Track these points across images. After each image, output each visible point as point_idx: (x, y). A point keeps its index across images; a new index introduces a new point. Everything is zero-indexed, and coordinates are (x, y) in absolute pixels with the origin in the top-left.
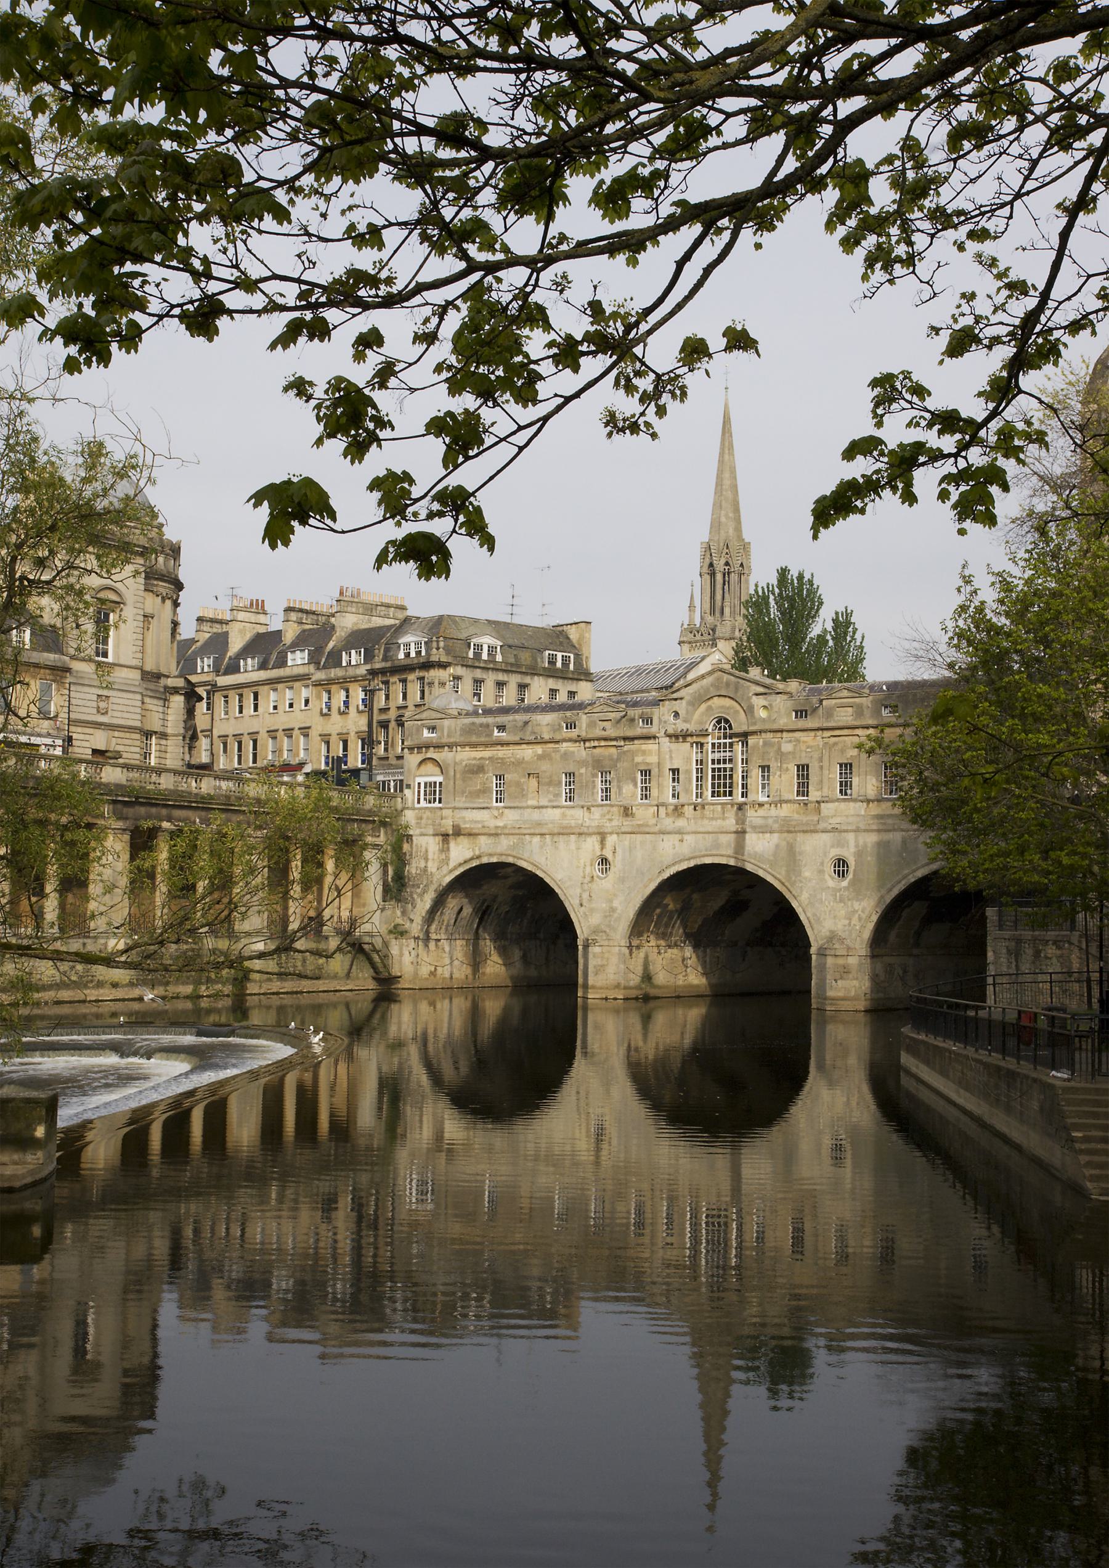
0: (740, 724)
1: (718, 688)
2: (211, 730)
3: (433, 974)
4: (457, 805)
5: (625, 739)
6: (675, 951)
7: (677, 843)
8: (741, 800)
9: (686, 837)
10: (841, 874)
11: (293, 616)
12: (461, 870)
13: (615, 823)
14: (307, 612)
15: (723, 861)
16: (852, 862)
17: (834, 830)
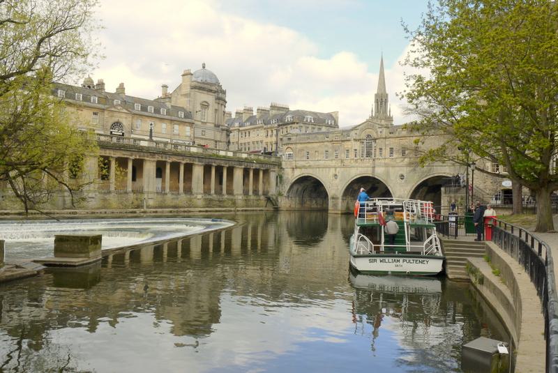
0: (375, 135)
3: (290, 206)
11: (260, 111)
16: (405, 175)
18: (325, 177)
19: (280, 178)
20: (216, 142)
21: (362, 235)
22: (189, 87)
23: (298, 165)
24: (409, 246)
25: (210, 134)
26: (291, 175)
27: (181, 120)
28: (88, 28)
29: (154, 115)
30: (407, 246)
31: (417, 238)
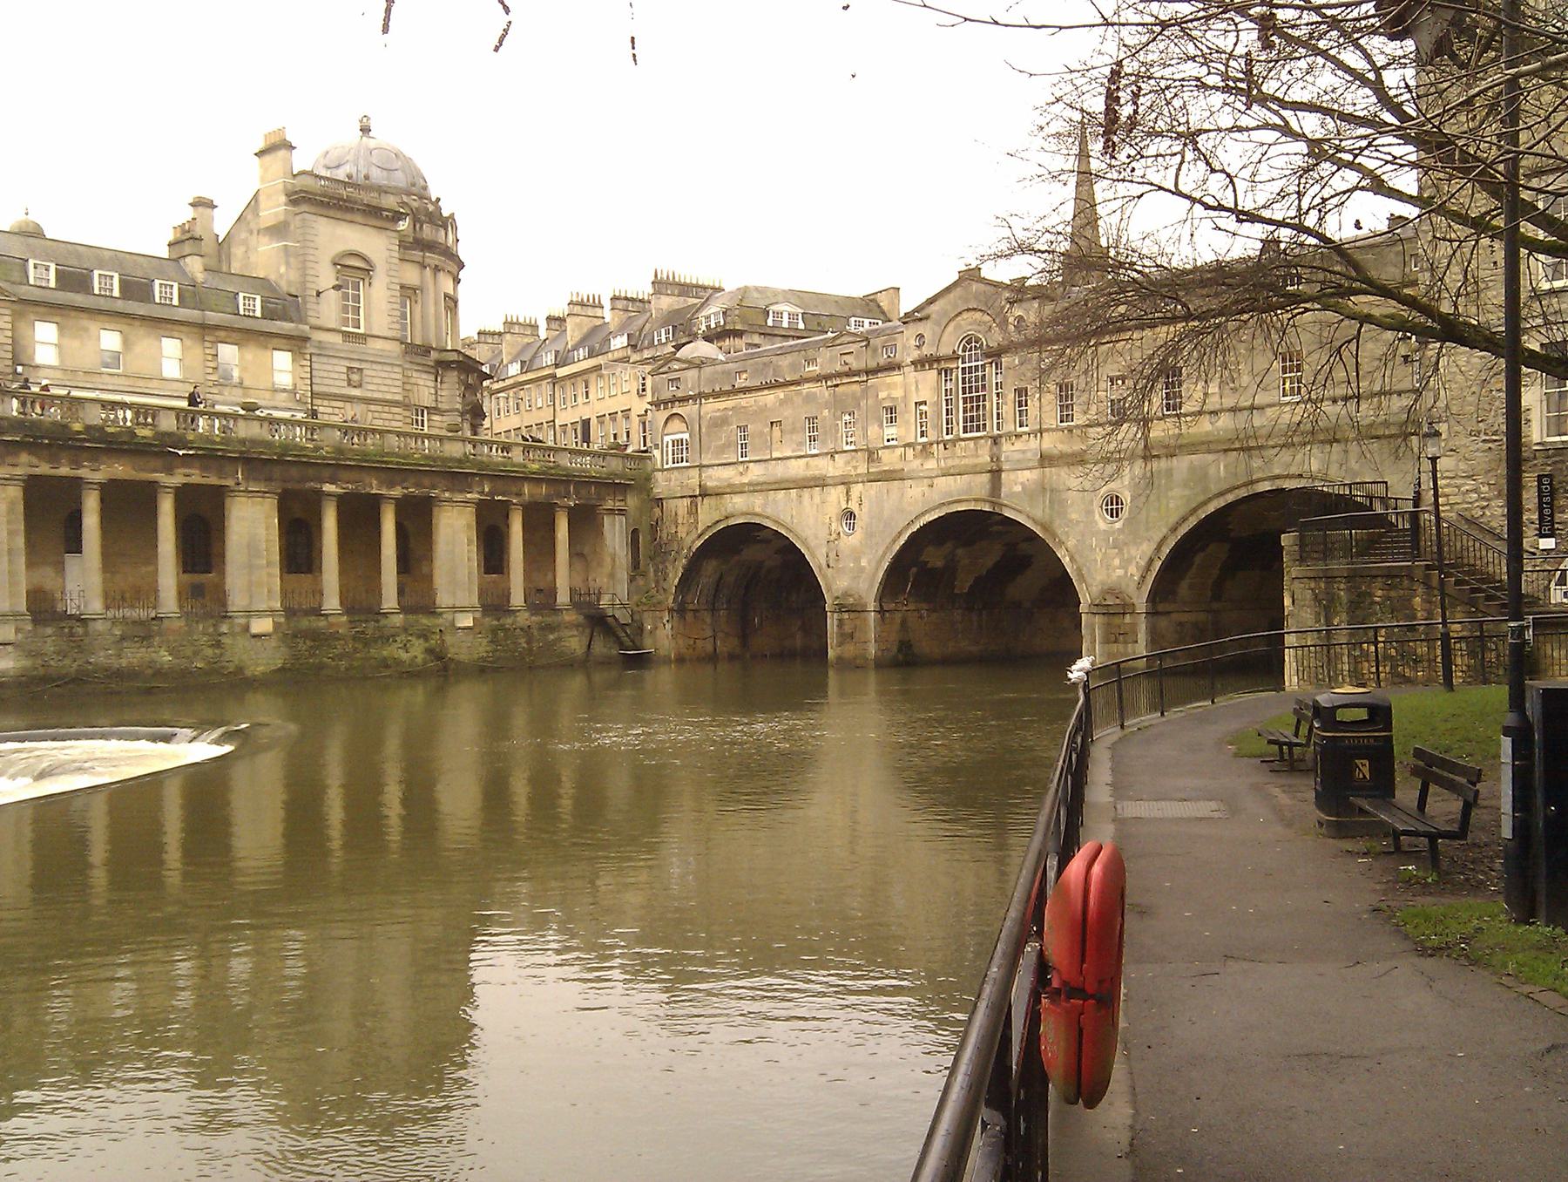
1: (966, 301)
2: (554, 421)
4: (705, 462)
5: (867, 373)
7: (926, 489)
8: (996, 432)
9: (936, 481)
10: (1114, 513)
11: (620, 304)
13: (862, 469)
14: (632, 300)
16: (1126, 497)
22: (283, 199)
25: (383, 382)
27: (248, 324)
28: (910, 452)
29: (121, 306)
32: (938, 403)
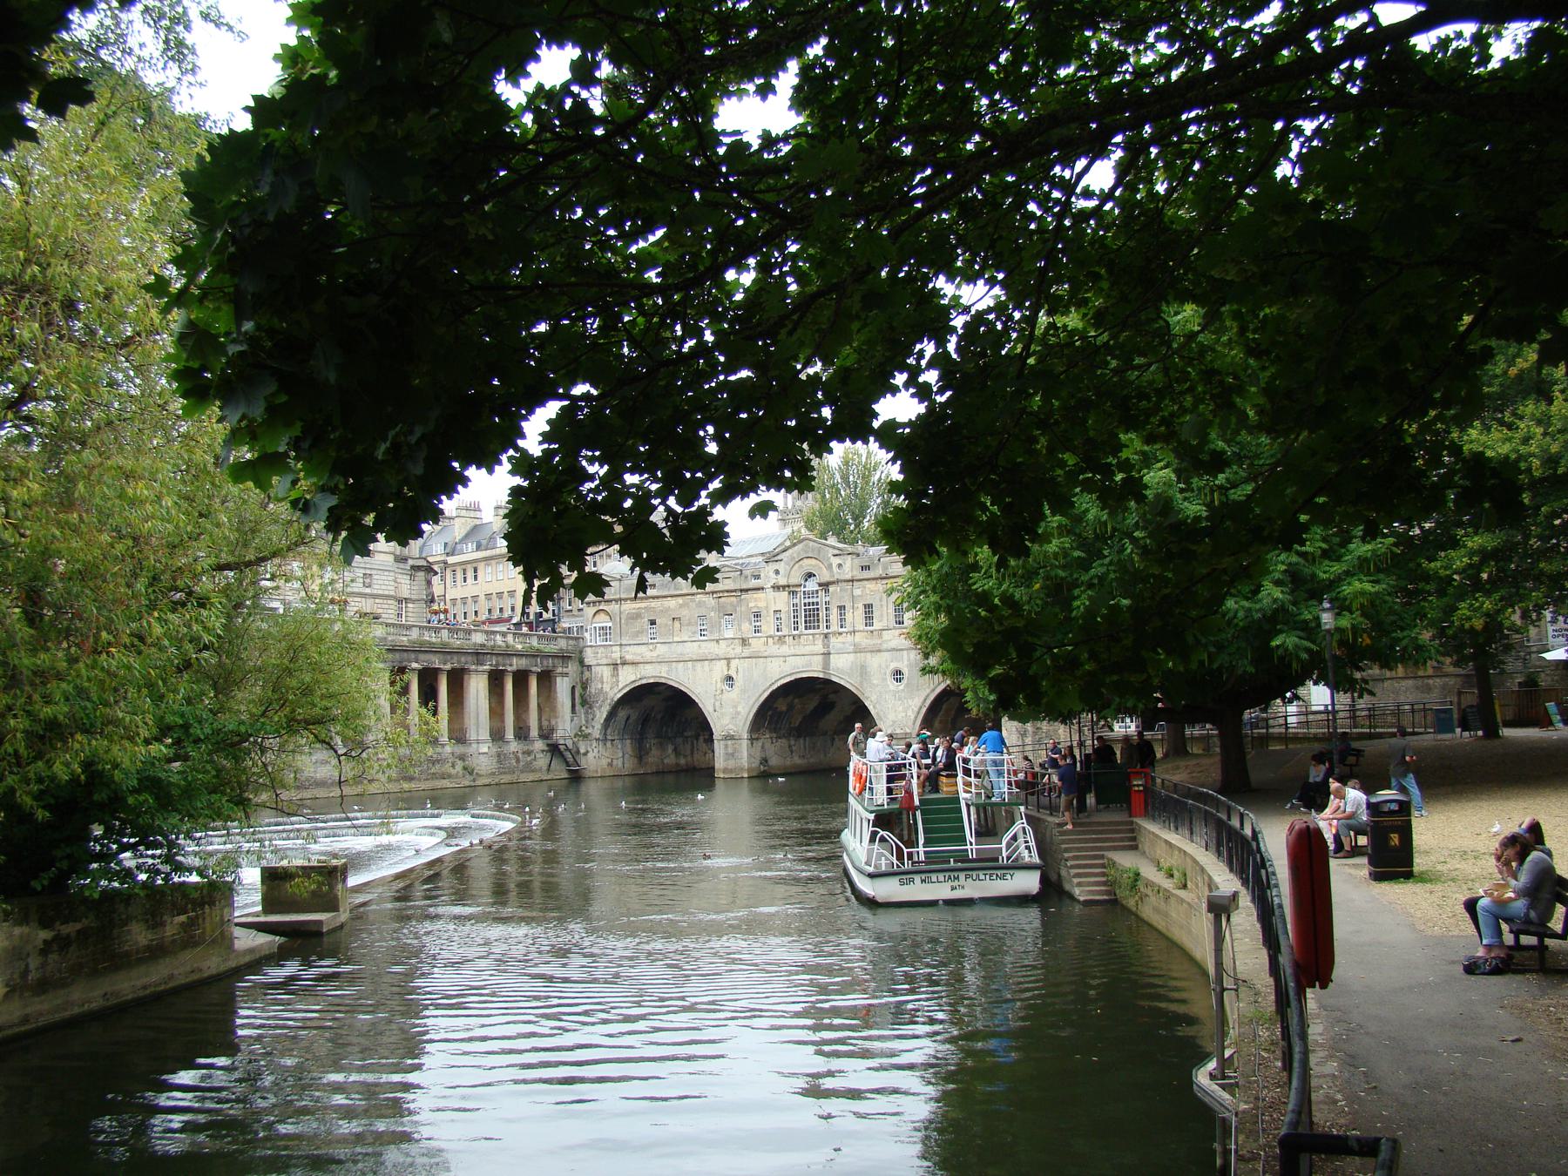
1: (806, 552)
3: (610, 765)
6: (784, 740)
8: (826, 631)
12: (628, 689)
15: (815, 675)
16: (905, 671)
17: (893, 650)
18: (701, 685)
19: (583, 698)
20: (400, 601)
21: (882, 833)
23: (629, 657)
24: (972, 846)
26: (612, 685)
28: (770, 640)
30: (969, 847)
31: (987, 830)
32: (789, 611)
